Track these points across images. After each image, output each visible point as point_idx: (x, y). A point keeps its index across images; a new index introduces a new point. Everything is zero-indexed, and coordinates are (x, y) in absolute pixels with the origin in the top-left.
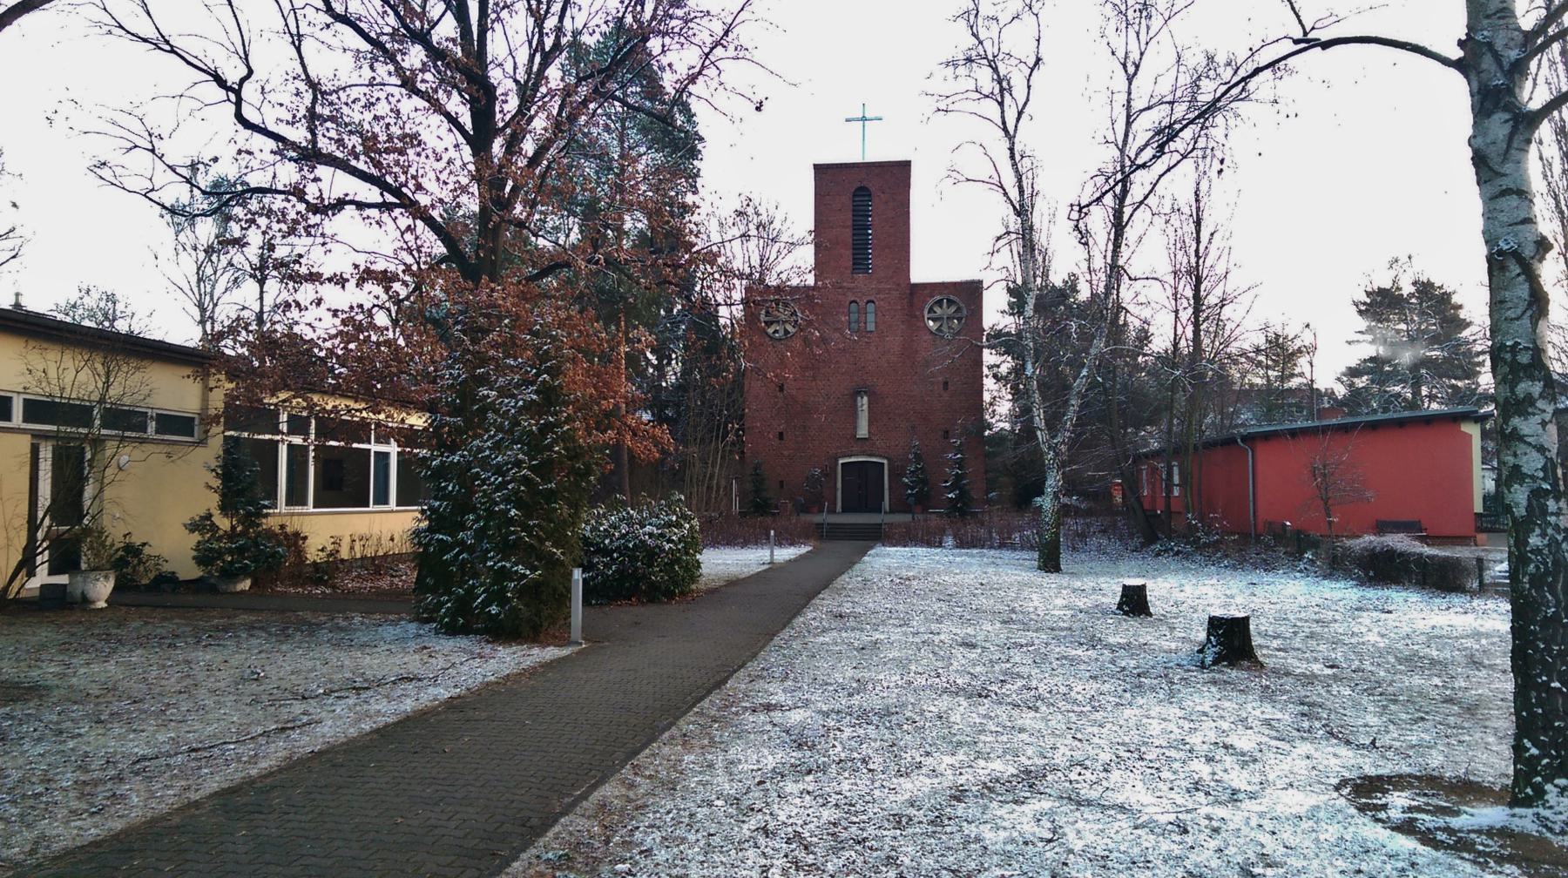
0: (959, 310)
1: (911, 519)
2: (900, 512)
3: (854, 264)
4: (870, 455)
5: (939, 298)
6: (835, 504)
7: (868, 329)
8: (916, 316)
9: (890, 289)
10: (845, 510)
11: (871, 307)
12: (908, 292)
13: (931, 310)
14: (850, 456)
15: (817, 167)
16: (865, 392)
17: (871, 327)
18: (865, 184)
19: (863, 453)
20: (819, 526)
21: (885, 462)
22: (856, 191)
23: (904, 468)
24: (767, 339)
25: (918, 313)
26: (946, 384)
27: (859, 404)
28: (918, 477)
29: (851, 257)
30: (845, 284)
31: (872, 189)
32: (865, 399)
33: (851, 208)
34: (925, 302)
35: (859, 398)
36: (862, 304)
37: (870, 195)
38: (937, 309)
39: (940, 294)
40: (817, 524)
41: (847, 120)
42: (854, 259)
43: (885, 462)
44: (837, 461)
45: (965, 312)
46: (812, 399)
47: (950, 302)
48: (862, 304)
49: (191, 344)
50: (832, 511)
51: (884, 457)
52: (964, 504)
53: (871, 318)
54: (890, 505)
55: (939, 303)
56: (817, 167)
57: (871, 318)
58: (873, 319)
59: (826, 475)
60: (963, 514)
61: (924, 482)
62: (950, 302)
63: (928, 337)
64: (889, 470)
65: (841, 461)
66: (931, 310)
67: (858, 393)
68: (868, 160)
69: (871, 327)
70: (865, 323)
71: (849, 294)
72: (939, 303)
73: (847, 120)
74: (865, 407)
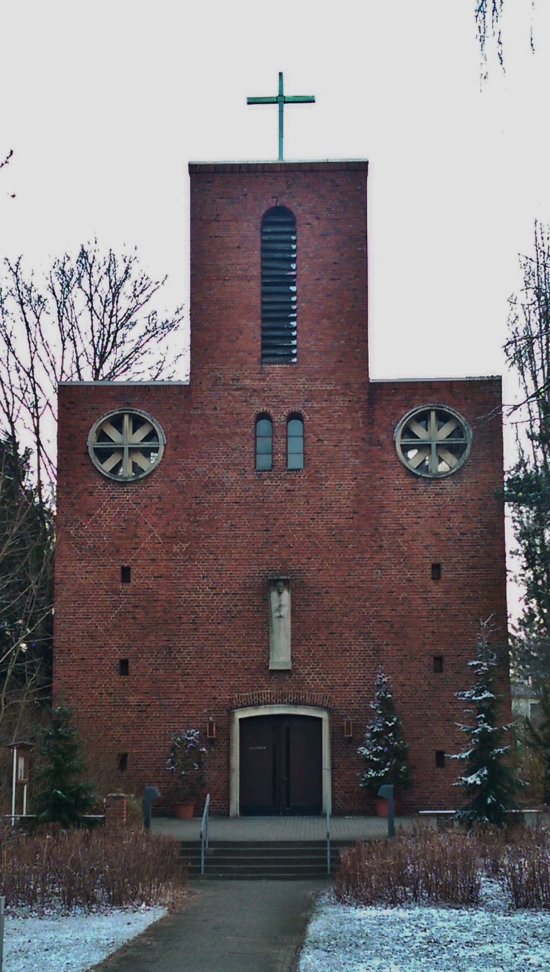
0: (459, 432)
1: (386, 831)
2: (353, 813)
3: (264, 347)
4: (296, 703)
5: (420, 409)
6: (227, 799)
7: (290, 466)
8: (379, 443)
9: (330, 393)
10: (249, 810)
11: (295, 427)
12: (365, 397)
13: (408, 432)
14: (256, 705)
15: (197, 172)
16: (286, 582)
17: (296, 462)
18: (284, 201)
19: (280, 699)
20: (191, 848)
21: (324, 715)
22: (265, 216)
23: (359, 728)
24: (100, 483)
25: (383, 437)
26: (436, 567)
27: (274, 605)
28: (387, 745)
29: (258, 334)
30: (247, 382)
31: (298, 211)
32: (286, 596)
33: (259, 244)
34: (396, 417)
35: (274, 595)
36: (279, 419)
37: (293, 223)
38: (418, 430)
39: (424, 402)
40: (185, 844)
41: (281, 74)
42: (263, 337)
43: (324, 715)
44: (230, 713)
45: (470, 434)
46: (185, 595)
47: (443, 418)
48: (279, 419)
49: (370, 376)
50: (221, 812)
51: (322, 707)
52: (500, 798)
53: (296, 445)
54: (334, 799)
55: (117, 422)
56: (197, 172)
57: (296, 445)
58: (300, 449)
59: (211, 743)
60: (497, 815)
61: (400, 754)
62: (138, 422)
63: (401, 480)
64: (332, 733)
65: (240, 714)
66: (408, 432)
67: (273, 583)
68: (294, 154)
69: (296, 462)
70: (286, 454)
71: (256, 400)
72: (422, 418)
73: (281, 74)
74: (286, 611)
